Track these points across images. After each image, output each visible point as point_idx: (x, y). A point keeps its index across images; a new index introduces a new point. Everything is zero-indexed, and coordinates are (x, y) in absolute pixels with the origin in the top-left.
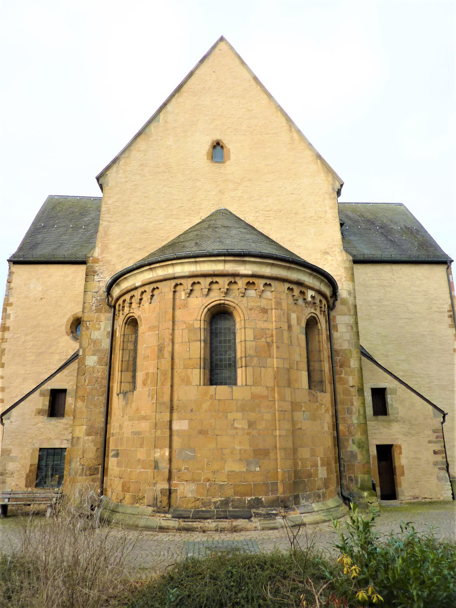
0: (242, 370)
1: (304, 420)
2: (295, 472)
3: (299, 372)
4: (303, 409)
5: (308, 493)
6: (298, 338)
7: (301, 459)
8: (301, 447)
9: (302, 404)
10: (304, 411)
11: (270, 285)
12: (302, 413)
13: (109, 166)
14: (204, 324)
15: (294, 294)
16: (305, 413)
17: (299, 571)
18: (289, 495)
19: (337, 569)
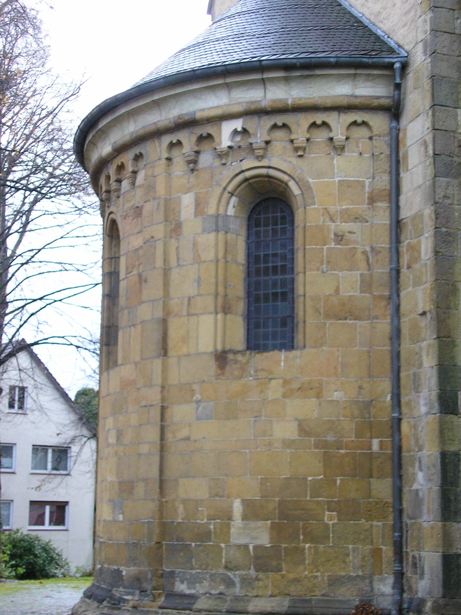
0: (217, 239)
1: (198, 419)
2: (164, 526)
3: (193, 319)
4: (198, 396)
5: (193, 572)
6: (195, 244)
7: (184, 502)
8: (186, 476)
9: (196, 387)
10: (198, 402)
11: (179, 143)
12: (194, 405)
13: (182, 82)
14: (341, 145)
15: (293, 137)
16: (202, 405)
17: (233, 573)
18: (147, 569)
19: (452, 134)
